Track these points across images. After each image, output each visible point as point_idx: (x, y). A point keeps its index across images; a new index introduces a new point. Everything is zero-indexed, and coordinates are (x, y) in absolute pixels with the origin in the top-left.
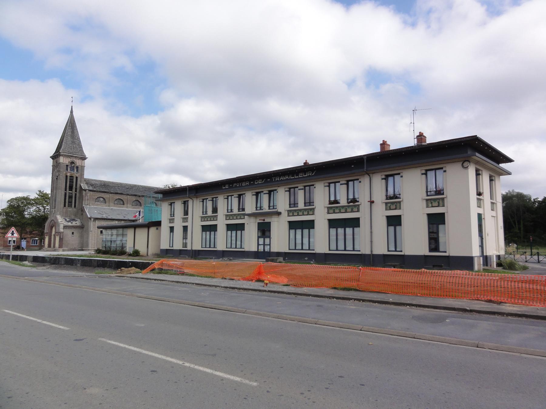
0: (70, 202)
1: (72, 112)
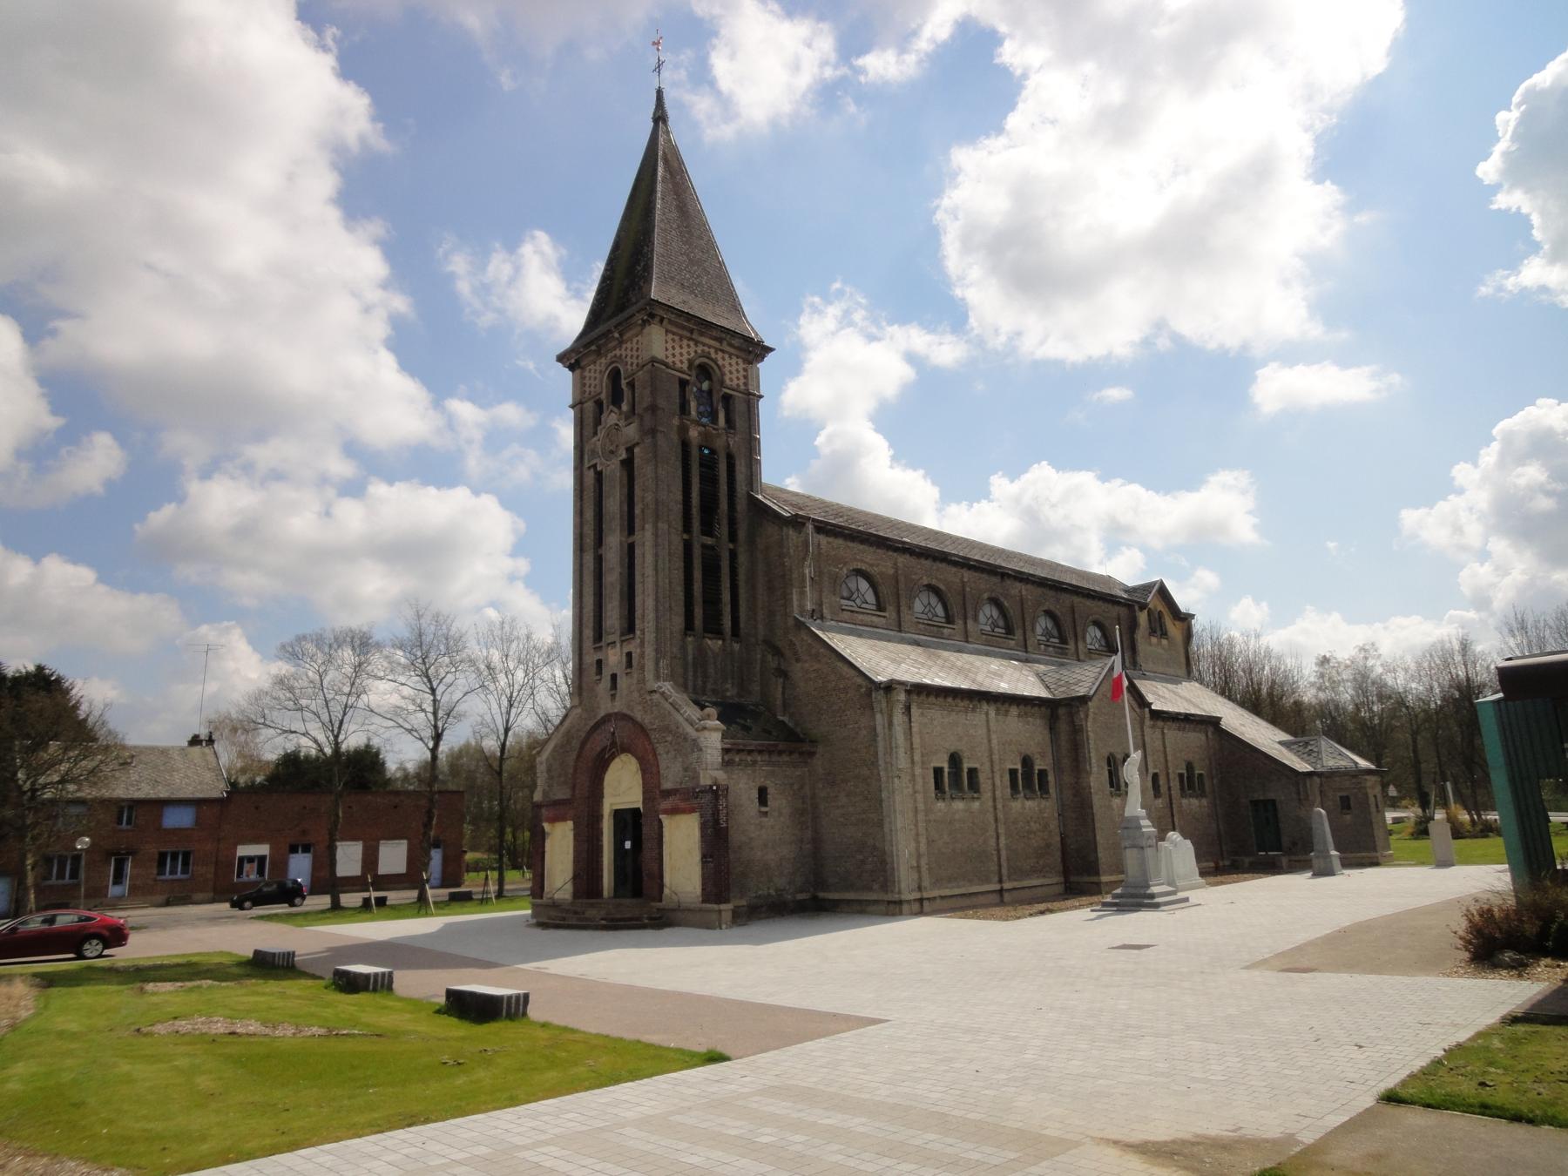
1: (660, 118)
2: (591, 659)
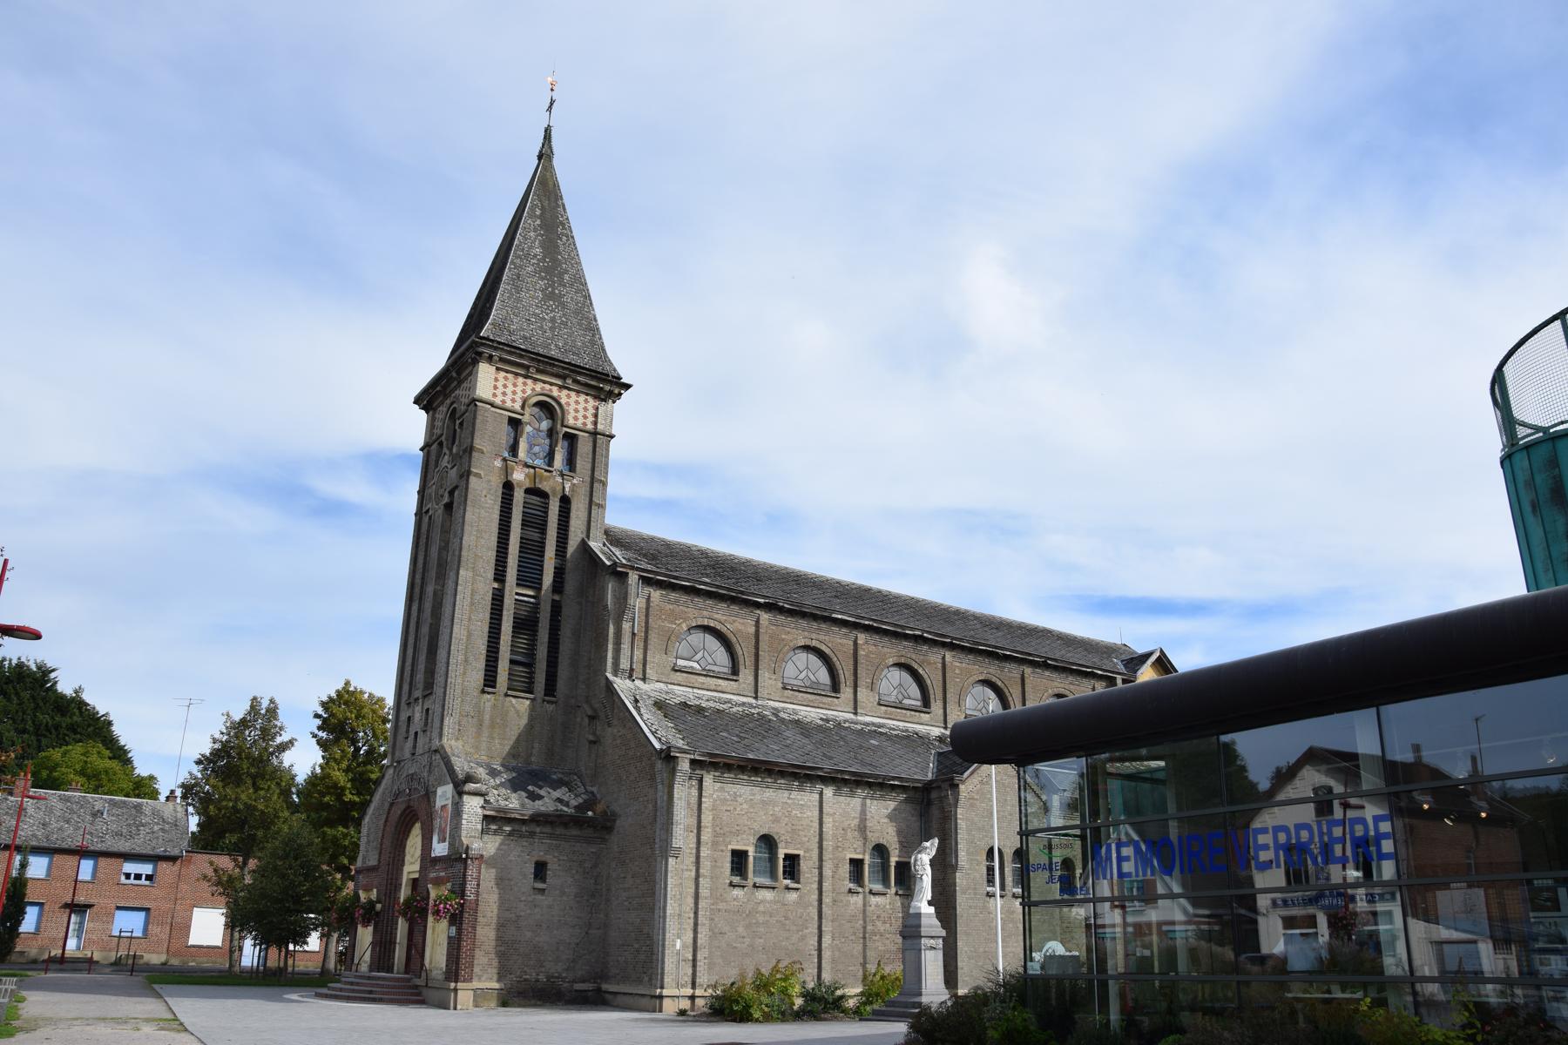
0: (525, 662)
1: (545, 155)
2: (403, 717)
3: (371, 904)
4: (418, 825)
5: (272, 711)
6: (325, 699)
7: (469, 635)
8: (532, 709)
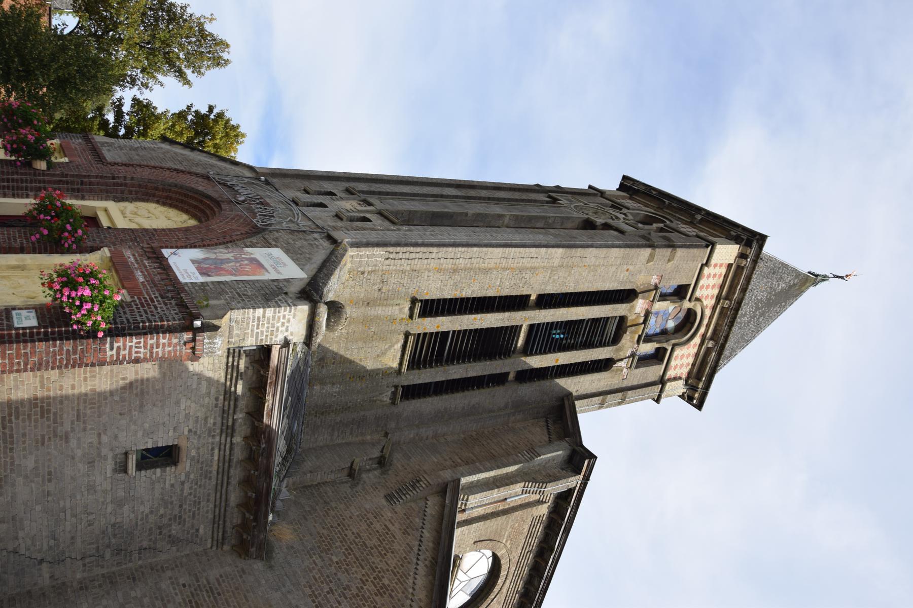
3: (45, 154)
4: (192, 222)
5: (218, 62)
6: (228, 115)
7: (486, 271)
8: (385, 373)
